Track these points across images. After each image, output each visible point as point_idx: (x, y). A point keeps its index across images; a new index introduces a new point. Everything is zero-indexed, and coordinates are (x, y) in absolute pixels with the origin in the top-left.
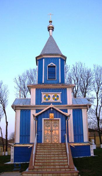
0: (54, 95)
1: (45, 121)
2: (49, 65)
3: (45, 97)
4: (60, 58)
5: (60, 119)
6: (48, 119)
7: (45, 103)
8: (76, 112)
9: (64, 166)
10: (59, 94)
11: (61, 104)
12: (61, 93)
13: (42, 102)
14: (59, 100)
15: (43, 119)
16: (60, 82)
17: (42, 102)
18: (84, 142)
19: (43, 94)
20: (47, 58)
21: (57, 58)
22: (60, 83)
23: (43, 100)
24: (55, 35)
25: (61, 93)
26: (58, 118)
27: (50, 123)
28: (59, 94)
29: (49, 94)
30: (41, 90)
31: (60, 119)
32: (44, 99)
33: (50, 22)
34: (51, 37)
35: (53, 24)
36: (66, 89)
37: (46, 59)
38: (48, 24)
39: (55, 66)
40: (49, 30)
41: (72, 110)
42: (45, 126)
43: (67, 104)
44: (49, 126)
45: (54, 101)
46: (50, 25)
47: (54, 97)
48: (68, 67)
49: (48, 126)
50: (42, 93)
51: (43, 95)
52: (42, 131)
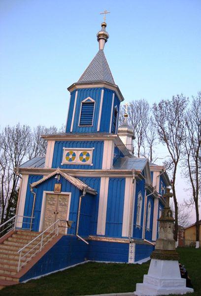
0: (82, 151)
1: (48, 195)
2: (84, 101)
3: (68, 155)
4: (104, 89)
5: (70, 194)
6: (52, 192)
7: (66, 166)
8: (115, 182)
9: (11, 272)
10: (91, 150)
11: (91, 169)
12: (94, 148)
13: (62, 164)
14: (89, 162)
15: (45, 192)
16: (98, 130)
17: (62, 164)
18: (122, 237)
19: (66, 150)
20: (82, 89)
21: (97, 89)
22: (98, 132)
23: (65, 161)
24: (109, 50)
25: (94, 148)
26: (49, 190)
27: (55, 200)
28: (91, 150)
29: (88, 151)
30: (81, 144)
31: (70, 194)
32: (65, 159)
33: (102, 26)
34: (101, 54)
35: (108, 30)
36: (102, 142)
37: (80, 90)
38: (99, 30)
39: (93, 103)
40: (99, 40)
41: (108, 180)
42: (47, 204)
43: (101, 169)
44: (53, 204)
45: (81, 162)
46: (102, 31)
47: (81, 155)
48: (187, 100)
49: (51, 205)
50: (64, 148)
51: (65, 153)
52: (40, 211)
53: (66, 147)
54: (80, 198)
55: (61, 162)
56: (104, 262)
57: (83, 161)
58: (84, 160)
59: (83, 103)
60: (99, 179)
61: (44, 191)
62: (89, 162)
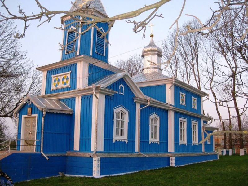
0: (64, 76)
1: (26, 118)
10: (69, 74)
14: (68, 85)
15: (23, 116)
17: (51, 90)
25: (71, 71)
27: (30, 122)
28: (69, 74)
31: (36, 115)
47: (63, 79)
50: (52, 76)
52: (21, 133)
53: (53, 75)
54: (43, 118)
55: (51, 89)
56: (89, 176)
57: (64, 85)
58: (65, 84)
59: (69, 33)
60: (73, 99)
61: (208, 143)
62: (68, 85)
